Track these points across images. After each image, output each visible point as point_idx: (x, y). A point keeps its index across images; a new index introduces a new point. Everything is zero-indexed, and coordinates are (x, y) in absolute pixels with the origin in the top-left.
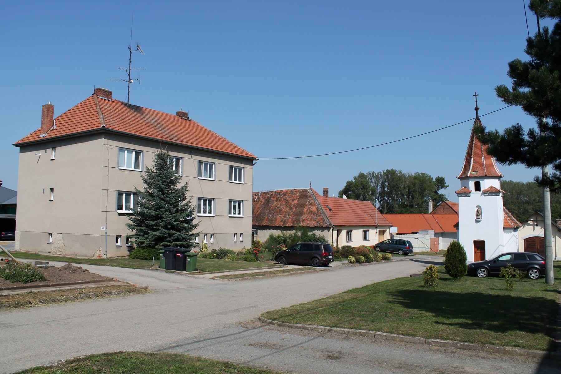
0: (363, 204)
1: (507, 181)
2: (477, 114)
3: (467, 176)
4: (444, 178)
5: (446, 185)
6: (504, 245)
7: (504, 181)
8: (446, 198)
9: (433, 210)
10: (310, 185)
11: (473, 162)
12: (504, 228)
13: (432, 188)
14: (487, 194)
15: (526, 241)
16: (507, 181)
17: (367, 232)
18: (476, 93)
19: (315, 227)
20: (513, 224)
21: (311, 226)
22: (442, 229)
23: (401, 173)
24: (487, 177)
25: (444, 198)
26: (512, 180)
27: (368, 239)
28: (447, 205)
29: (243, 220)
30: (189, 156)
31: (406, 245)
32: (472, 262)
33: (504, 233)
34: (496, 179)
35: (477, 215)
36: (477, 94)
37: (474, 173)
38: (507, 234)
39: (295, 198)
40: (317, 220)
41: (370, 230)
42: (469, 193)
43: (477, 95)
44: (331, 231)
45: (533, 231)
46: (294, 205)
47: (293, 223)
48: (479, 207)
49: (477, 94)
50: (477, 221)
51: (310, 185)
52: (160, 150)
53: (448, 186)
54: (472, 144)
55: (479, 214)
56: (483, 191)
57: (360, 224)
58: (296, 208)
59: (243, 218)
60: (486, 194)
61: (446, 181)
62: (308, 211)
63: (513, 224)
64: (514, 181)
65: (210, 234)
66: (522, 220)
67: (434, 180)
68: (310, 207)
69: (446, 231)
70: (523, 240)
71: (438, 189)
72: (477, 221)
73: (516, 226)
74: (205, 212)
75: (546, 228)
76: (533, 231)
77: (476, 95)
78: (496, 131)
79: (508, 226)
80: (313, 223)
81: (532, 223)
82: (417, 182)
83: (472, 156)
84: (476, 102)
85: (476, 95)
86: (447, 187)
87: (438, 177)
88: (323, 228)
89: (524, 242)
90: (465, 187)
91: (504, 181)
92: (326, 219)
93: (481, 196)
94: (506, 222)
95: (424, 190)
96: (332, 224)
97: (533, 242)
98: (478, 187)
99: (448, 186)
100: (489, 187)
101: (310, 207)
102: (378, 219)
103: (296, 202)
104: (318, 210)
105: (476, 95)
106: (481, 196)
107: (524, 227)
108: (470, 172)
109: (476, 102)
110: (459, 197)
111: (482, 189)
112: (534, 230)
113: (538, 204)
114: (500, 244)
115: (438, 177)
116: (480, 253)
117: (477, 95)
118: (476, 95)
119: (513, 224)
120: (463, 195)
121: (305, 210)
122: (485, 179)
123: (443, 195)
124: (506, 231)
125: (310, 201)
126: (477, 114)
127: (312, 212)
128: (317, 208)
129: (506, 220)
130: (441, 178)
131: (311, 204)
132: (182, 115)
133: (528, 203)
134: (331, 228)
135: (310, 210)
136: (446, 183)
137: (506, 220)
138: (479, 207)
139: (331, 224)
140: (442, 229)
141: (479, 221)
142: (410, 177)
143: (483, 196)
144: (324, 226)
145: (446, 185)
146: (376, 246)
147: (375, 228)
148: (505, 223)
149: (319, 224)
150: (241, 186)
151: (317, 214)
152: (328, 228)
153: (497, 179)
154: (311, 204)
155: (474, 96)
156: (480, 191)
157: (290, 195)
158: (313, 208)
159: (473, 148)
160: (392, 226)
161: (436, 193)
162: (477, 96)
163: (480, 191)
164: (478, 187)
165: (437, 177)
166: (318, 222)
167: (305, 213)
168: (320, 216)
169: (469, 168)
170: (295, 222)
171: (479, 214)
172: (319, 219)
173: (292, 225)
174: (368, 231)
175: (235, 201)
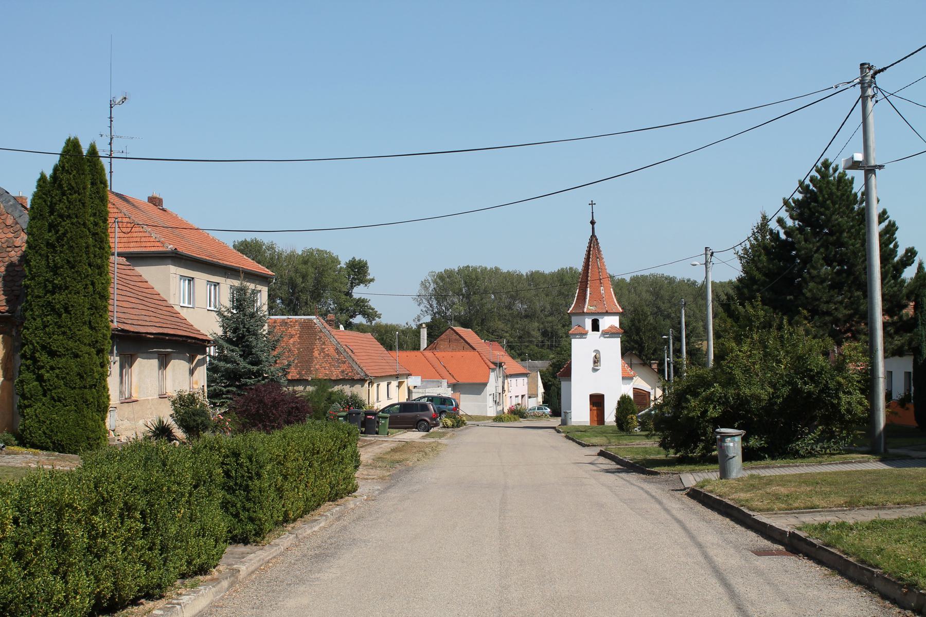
0: (365, 339)
1: (489, 268)
2: (593, 229)
3: (583, 312)
4: (366, 264)
5: (368, 277)
8: (370, 306)
9: (428, 346)
11: (590, 294)
12: (623, 378)
13: (341, 283)
19: (340, 380)
21: (333, 378)
22: (453, 377)
23: (273, 248)
24: (607, 313)
25: (367, 306)
26: (498, 266)
28: (457, 334)
31: (452, 405)
35: (595, 362)
37: (591, 308)
39: (293, 332)
40: (342, 369)
41: (392, 382)
42: (586, 334)
44: (366, 385)
46: (294, 344)
47: (299, 373)
48: (597, 351)
50: (595, 370)
52: (239, 282)
53: (372, 280)
54: (588, 270)
55: (596, 361)
56: (603, 331)
58: (298, 349)
62: (322, 354)
64: (504, 269)
66: (533, 355)
67: (343, 265)
68: (324, 349)
69: (461, 381)
71: (352, 287)
72: (595, 370)
77: (592, 204)
80: (336, 374)
82: (311, 270)
83: (588, 286)
84: (593, 213)
85: (592, 204)
86: (372, 283)
88: (352, 382)
90: (579, 326)
92: (356, 367)
95: (324, 287)
96: (369, 375)
98: (595, 327)
99: (372, 280)
101: (324, 349)
102: (395, 364)
103: (296, 339)
104: (339, 353)
105: (592, 204)
108: (586, 306)
109: (593, 213)
111: (601, 329)
113: (550, 319)
118: (592, 204)
121: (316, 353)
123: (363, 301)
125: (320, 338)
126: (593, 229)
127: (328, 355)
128: (337, 349)
130: (360, 262)
131: (324, 343)
132: (155, 201)
133: (529, 316)
134: (367, 380)
135: (324, 352)
138: (597, 351)
139: (367, 375)
140: (453, 377)
141: (598, 370)
142: (291, 257)
143: (602, 338)
144: (355, 378)
145: (368, 277)
149: (347, 374)
151: (338, 359)
152: (362, 381)
154: (324, 343)
156: (598, 331)
157: (283, 328)
158: (330, 350)
159: (589, 275)
160: (410, 375)
161: (348, 294)
163: (598, 331)
164: (595, 327)
166: (343, 372)
167: (316, 358)
168: (344, 363)
169: (585, 301)
170: (303, 372)
171: (596, 361)
172: (343, 367)
173: (298, 376)
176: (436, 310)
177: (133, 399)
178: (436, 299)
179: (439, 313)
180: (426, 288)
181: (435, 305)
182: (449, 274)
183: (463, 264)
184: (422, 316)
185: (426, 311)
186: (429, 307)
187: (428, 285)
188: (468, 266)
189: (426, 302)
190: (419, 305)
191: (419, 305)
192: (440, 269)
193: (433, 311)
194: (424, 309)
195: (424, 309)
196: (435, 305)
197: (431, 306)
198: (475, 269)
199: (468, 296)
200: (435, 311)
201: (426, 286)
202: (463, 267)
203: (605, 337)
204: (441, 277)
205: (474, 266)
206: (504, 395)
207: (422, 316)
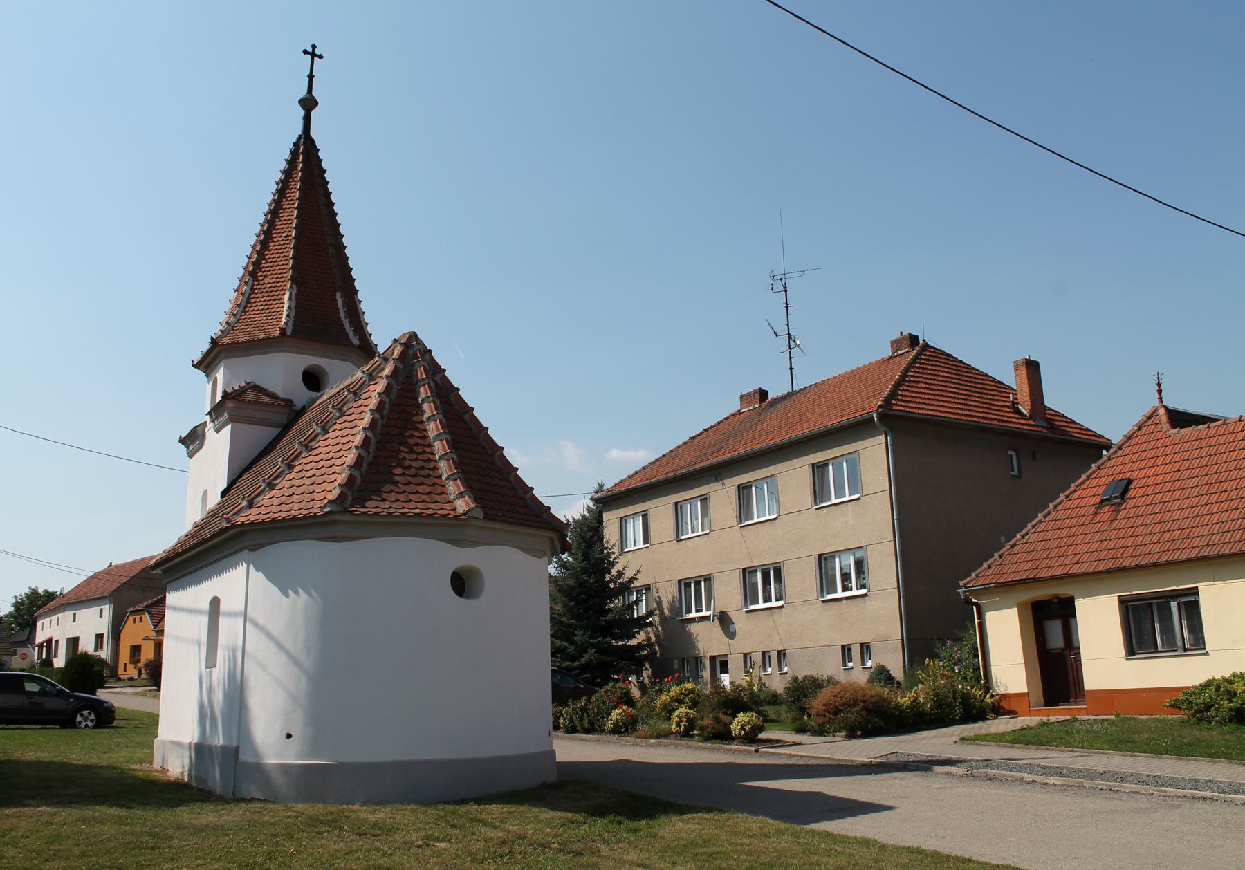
10: (1160, 392)
18: (305, 52)
29: (868, 603)
30: (718, 485)
36: (310, 50)
43: (314, 50)
45: (206, 490)
49: (310, 50)
51: (1160, 392)
59: (783, 609)
65: (742, 655)
74: (845, 589)
75: (1145, 419)
76: (206, 490)
77: (313, 55)
78: (30, 588)
84: (311, 77)
105: (313, 54)
109: (311, 77)
117: (314, 50)
126: (307, 120)
150: (850, 509)
175: (832, 554)
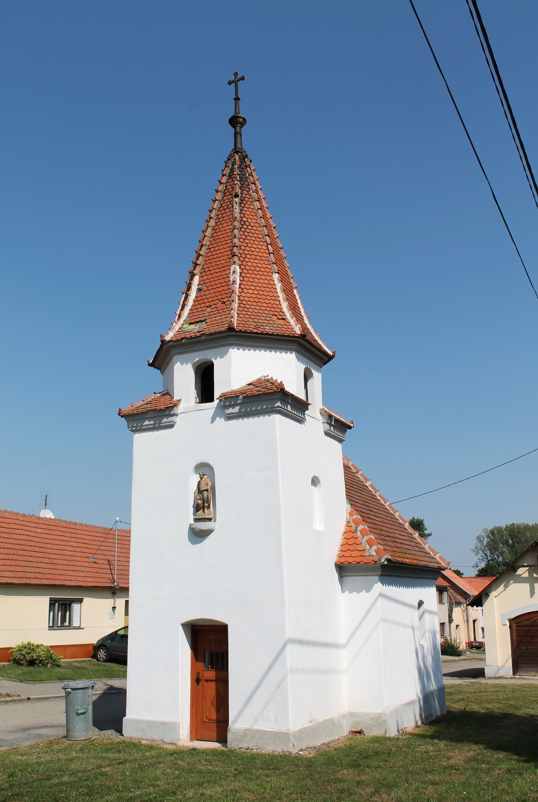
4: (422, 521)
6: (342, 639)
7: (524, 525)
11: (199, 290)
14: (236, 409)
15: (514, 625)
16: (531, 525)
17: (76, 607)
18: (236, 74)
20: (376, 551)
27: (76, 624)
32: (173, 727)
33: (343, 591)
34: (287, 350)
35: (197, 508)
36: (239, 76)
38: (355, 594)
45: (531, 596)
53: (430, 535)
57: (34, 582)
60: (231, 410)
61: (426, 525)
63: (376, 551)
70: (508, 623)
73: (388, 556)
76: (531, 596)
79: (353, 558)
81: (526, 575)
86: (429, 537)
87: (413, 518)
89: (510, 627)
91: (524, 525)
93: (213, 420)
94: (352, 541)
97: (532, 626)
99: (430, 535)
100: (249, 381)
106: (213, 420)
107: (506, 587)
110: (135, 431)
112: (534, 593)
114: (289, 633)
115: (413, 518)
116: (213, 684)
119: (374, 548)
120: (147, 422)
122: (230, 345)
124: (349, 580)
129: (351, 535)
130: (418, 520)
136: (426, 529)
137: (351, 535)
141: (210, 532)
143: (220, 421)
145: (426, 532)
146: (99, 644)
147: (109, 594)
148: (346, 547)
153: (291, 350)
155: (230, 83)
162: (240, 83)
165: (411, 519)
174: (80, 601)
176: (489, 558)
177: (82, 627)
178: (489, 549)
179: (492, 560)
180: (481, 541)
181: (489, 554)
182: (499, 530)
183: (509, 523)
184: (479, 563)
185: (482, 559)
186: (484, 556)
187: (482, 539)
188: (513, 524)
189: (482, 553)
190: (476, 554)
191: (476, 554)
192: (490, 527)
193: (487, 558)
194: (481, 558)
195: (481, 558)
196: (489, 554)
197: (485, 555)
198: (518, 527)
199: (512, 546)
200: (489, 559)
201: (481, 540)
202: (510, 525)
203: (230, 417)
204: (492, 532)
205: (518, 523)
206: (453, 625)
207: (479, 563)
